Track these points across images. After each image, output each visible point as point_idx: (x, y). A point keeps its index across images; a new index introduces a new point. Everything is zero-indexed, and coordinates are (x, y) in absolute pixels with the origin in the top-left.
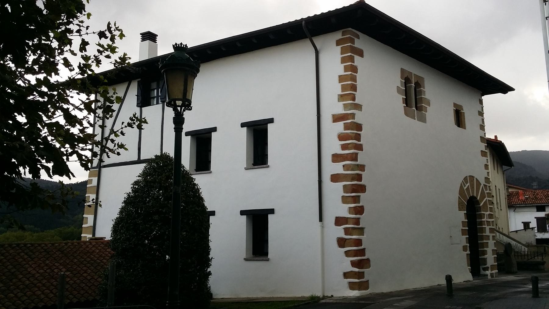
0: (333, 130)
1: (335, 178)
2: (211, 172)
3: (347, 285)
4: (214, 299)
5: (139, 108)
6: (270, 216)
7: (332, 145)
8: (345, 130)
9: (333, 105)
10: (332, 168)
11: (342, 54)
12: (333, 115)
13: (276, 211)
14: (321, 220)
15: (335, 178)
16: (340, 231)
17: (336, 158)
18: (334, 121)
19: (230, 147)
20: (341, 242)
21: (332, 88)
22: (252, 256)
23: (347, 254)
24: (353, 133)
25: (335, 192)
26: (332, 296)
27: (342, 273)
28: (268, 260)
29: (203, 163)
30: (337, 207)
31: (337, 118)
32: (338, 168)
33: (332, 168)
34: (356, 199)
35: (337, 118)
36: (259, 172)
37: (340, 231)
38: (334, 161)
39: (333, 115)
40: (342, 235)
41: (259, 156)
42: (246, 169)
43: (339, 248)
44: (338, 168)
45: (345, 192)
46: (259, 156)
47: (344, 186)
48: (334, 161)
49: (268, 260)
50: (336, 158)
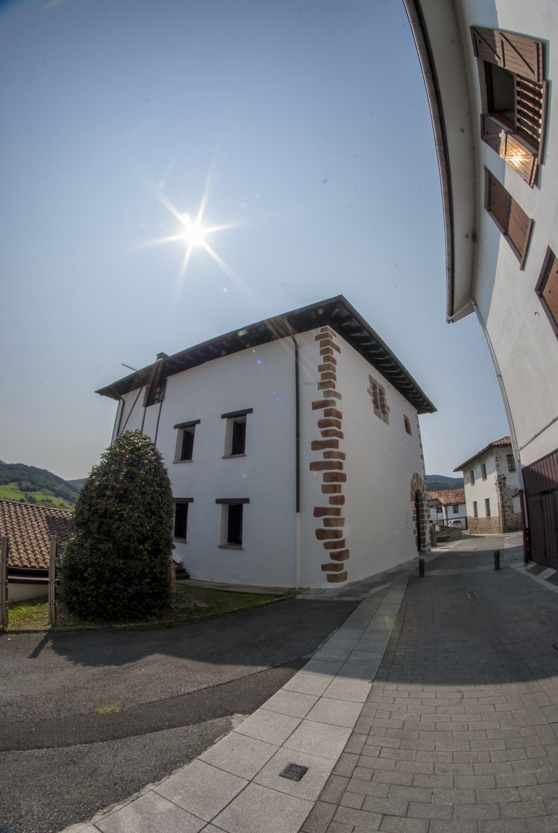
0: (312, 418)
1: (315, 466)
2: (192, 461)
3: (326, 578)
4: (192, 580)
5: (144, 408)
6: (245, 505)
7: (312, 432)
8: (325, 416)
9: (312, 393)
10: (311, 456)
11: (321, 347)
12: (313, 403)
13: (251, 501)
14: (298, 510)
15: (315, 466)
16: (319, 523)
17: (316, 445)
18: (313, 409)
19: (213, 438)
20: (320, 534)
21: (311, 375)
22: (227, 543)
23: (327, 546)
24: (331, 422)
25: (314, 480)
26: (308, 589)
27: (320, 566)
28: (242, 549)
29: (186, 452)
30: (315, 493)
31: (316, 406)
32: (319, 456)
33: (311, 456)
34: (336, 489)
35: (316, 406)
36: (237, 461)
37: (319, 523)
38: (313, 449)
39: (313, 403)
40: (322, 526)
41: (238, 445)
42: (174, 463)
43: (317, 540)
44: (319, 456)
45: (325, 480)
46: (238, 445)
47: (325, 475)
48: (313, 449)
49: (242, 549)
50: (316, 445)
